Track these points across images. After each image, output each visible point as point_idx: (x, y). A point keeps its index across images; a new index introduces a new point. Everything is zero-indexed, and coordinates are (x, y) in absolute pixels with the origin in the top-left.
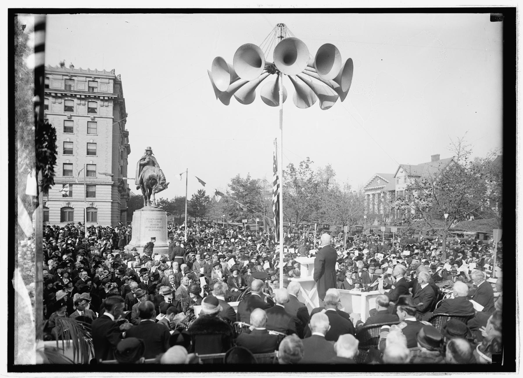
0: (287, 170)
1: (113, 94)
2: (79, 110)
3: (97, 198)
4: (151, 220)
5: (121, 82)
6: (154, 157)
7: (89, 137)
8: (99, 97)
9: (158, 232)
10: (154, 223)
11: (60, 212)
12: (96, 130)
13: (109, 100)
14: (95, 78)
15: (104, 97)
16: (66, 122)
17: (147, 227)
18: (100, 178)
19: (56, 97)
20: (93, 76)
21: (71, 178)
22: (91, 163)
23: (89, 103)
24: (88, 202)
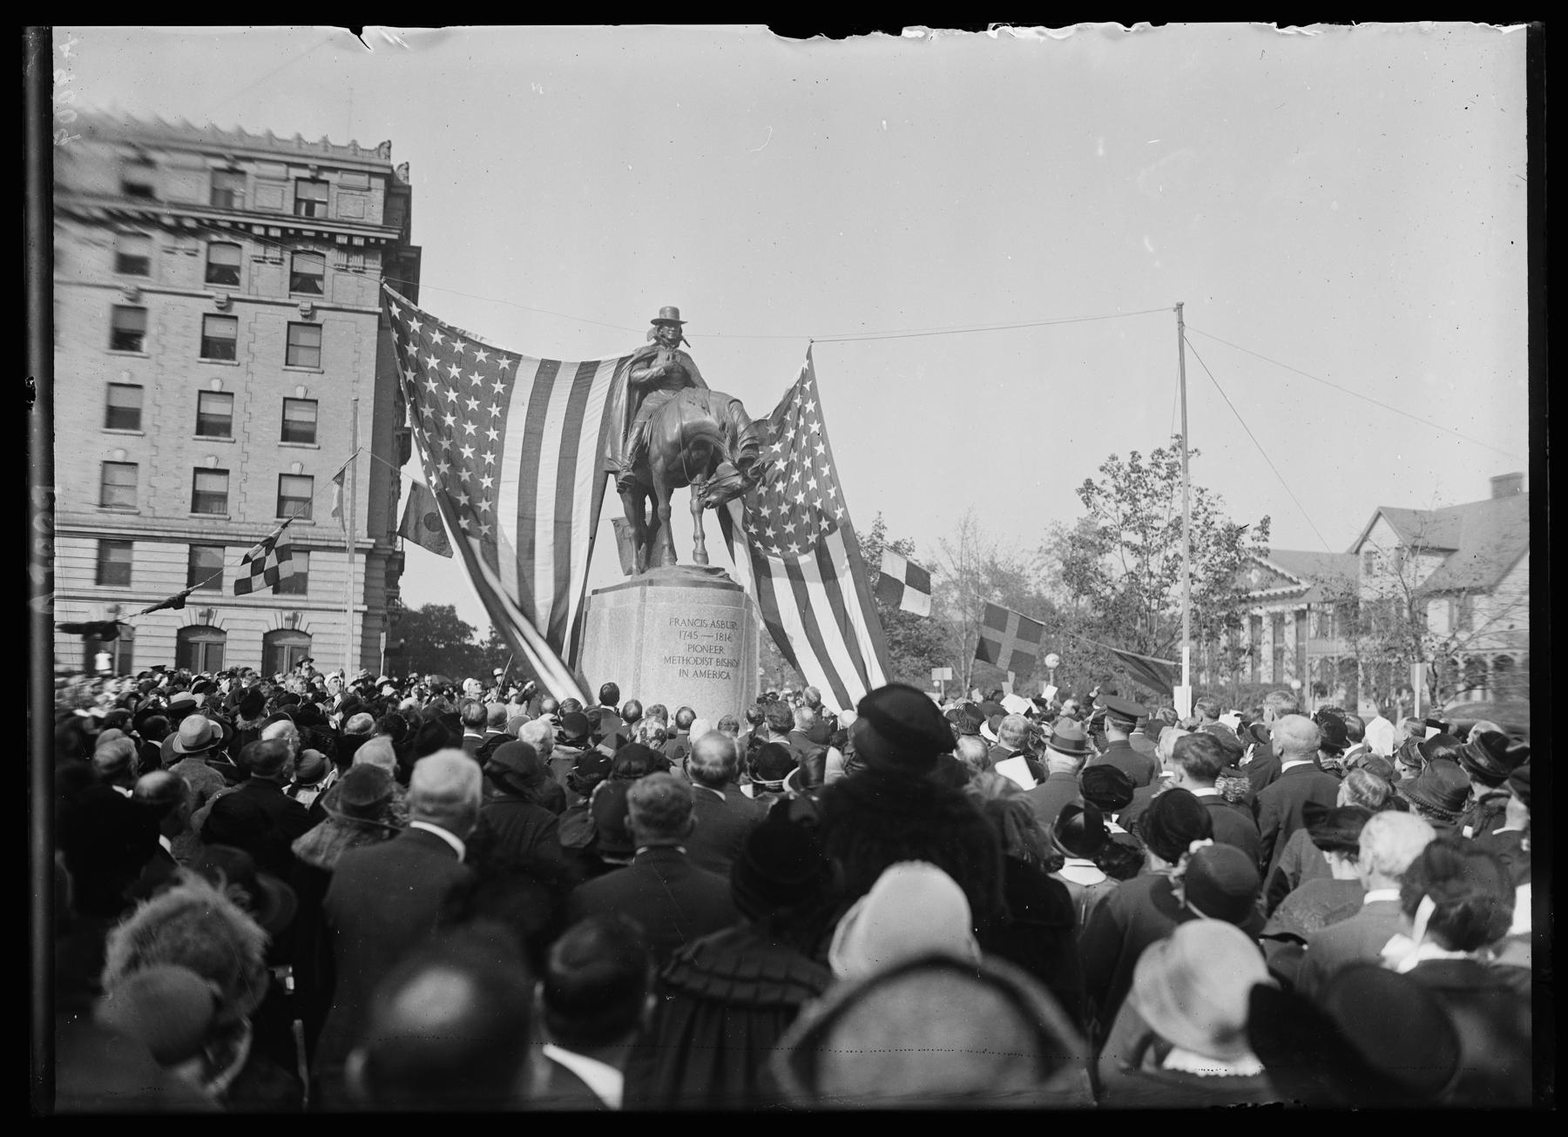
1: (382, 229)
2: (257, 281)
3: (311, 595)
4: (690, 629)
5: (410, 187)
6: (687, 356)
7: (292, 376)
9: (721, 683)
11: (174, 643)
12: (315, 353)
13: (370, 248)
14: (321, 169)
15: (350, 237)
16: (209, 321)
17: (670, 660)
18: (324, 522)
19: (178, 230)
20: (313, 163)
21: (221, 523)
22: (296, 470)
24: (278, 612)
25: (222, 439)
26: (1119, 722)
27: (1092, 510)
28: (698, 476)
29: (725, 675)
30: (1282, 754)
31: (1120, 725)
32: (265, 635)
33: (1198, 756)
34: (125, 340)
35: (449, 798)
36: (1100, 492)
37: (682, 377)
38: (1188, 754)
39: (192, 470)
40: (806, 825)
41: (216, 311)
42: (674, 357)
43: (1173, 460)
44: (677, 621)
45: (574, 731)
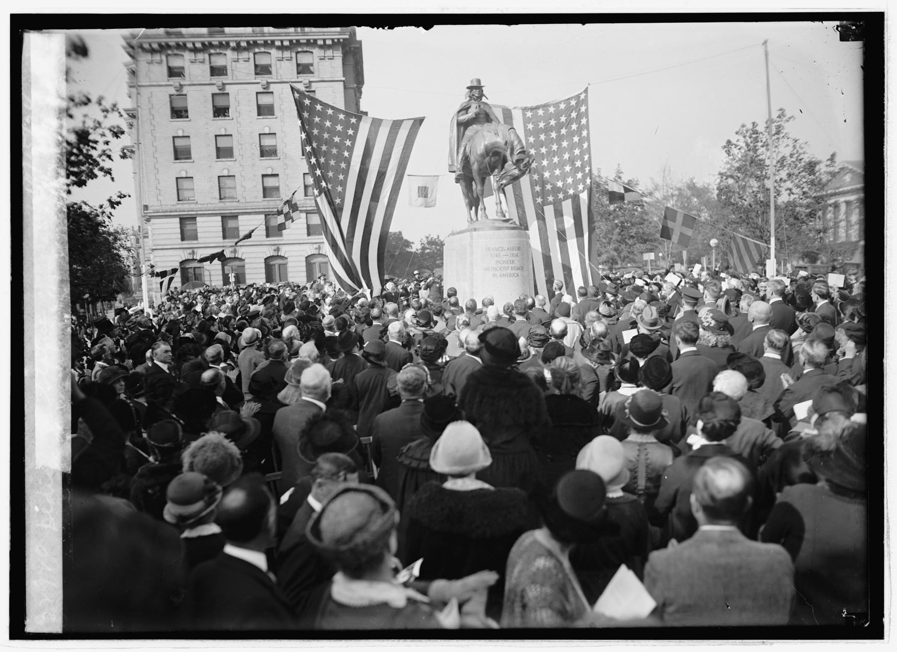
0: (738, 141)
2: (281, 72)
8: (315, 41)
10: (504, 259)
11: (263, 265)
12: (196, 269)
15: (324, 40)
16: (260, 96)
17: (487, 269)
23: (299, 55)
25: (273, 158)
26: (689, 301)
27: (731, 157)
28: (496, 170)
29: (516, 275)
30: (753, 321)
31: (689, 302)
32: (306, 258)
33: (685, 332)
34: (220, 111)
35: (315, 388)
36: (736, 146)
37: (484, 117)
38: (681, 332)
39: (261, 176)
40: (451, 396)
41: (262, 90)
42: (479, 106)
43: (779, 123)
44: (489, 249)
45: (424, 320)
